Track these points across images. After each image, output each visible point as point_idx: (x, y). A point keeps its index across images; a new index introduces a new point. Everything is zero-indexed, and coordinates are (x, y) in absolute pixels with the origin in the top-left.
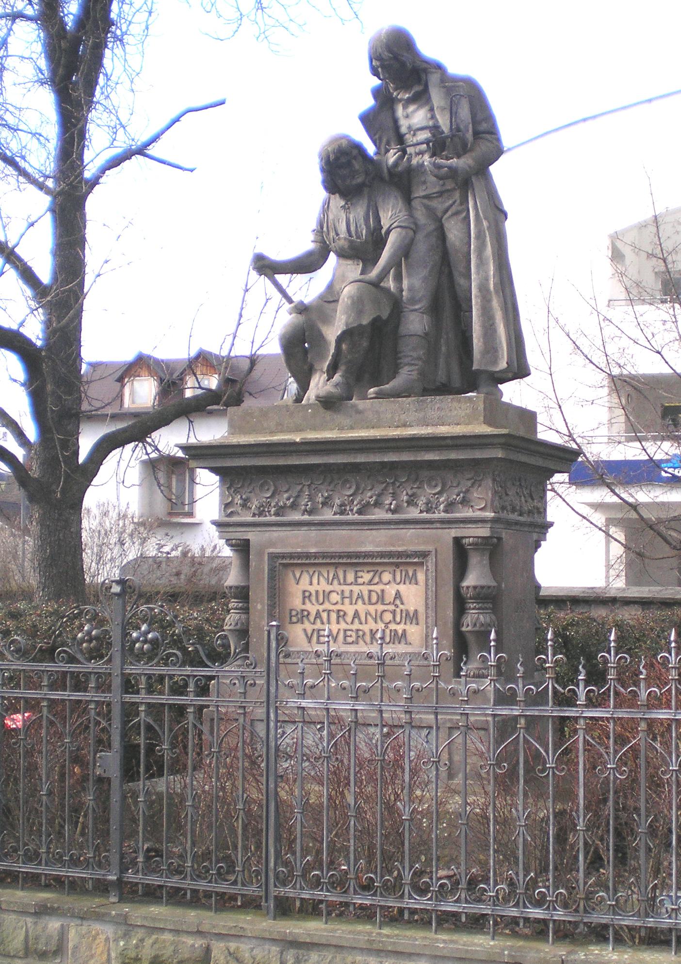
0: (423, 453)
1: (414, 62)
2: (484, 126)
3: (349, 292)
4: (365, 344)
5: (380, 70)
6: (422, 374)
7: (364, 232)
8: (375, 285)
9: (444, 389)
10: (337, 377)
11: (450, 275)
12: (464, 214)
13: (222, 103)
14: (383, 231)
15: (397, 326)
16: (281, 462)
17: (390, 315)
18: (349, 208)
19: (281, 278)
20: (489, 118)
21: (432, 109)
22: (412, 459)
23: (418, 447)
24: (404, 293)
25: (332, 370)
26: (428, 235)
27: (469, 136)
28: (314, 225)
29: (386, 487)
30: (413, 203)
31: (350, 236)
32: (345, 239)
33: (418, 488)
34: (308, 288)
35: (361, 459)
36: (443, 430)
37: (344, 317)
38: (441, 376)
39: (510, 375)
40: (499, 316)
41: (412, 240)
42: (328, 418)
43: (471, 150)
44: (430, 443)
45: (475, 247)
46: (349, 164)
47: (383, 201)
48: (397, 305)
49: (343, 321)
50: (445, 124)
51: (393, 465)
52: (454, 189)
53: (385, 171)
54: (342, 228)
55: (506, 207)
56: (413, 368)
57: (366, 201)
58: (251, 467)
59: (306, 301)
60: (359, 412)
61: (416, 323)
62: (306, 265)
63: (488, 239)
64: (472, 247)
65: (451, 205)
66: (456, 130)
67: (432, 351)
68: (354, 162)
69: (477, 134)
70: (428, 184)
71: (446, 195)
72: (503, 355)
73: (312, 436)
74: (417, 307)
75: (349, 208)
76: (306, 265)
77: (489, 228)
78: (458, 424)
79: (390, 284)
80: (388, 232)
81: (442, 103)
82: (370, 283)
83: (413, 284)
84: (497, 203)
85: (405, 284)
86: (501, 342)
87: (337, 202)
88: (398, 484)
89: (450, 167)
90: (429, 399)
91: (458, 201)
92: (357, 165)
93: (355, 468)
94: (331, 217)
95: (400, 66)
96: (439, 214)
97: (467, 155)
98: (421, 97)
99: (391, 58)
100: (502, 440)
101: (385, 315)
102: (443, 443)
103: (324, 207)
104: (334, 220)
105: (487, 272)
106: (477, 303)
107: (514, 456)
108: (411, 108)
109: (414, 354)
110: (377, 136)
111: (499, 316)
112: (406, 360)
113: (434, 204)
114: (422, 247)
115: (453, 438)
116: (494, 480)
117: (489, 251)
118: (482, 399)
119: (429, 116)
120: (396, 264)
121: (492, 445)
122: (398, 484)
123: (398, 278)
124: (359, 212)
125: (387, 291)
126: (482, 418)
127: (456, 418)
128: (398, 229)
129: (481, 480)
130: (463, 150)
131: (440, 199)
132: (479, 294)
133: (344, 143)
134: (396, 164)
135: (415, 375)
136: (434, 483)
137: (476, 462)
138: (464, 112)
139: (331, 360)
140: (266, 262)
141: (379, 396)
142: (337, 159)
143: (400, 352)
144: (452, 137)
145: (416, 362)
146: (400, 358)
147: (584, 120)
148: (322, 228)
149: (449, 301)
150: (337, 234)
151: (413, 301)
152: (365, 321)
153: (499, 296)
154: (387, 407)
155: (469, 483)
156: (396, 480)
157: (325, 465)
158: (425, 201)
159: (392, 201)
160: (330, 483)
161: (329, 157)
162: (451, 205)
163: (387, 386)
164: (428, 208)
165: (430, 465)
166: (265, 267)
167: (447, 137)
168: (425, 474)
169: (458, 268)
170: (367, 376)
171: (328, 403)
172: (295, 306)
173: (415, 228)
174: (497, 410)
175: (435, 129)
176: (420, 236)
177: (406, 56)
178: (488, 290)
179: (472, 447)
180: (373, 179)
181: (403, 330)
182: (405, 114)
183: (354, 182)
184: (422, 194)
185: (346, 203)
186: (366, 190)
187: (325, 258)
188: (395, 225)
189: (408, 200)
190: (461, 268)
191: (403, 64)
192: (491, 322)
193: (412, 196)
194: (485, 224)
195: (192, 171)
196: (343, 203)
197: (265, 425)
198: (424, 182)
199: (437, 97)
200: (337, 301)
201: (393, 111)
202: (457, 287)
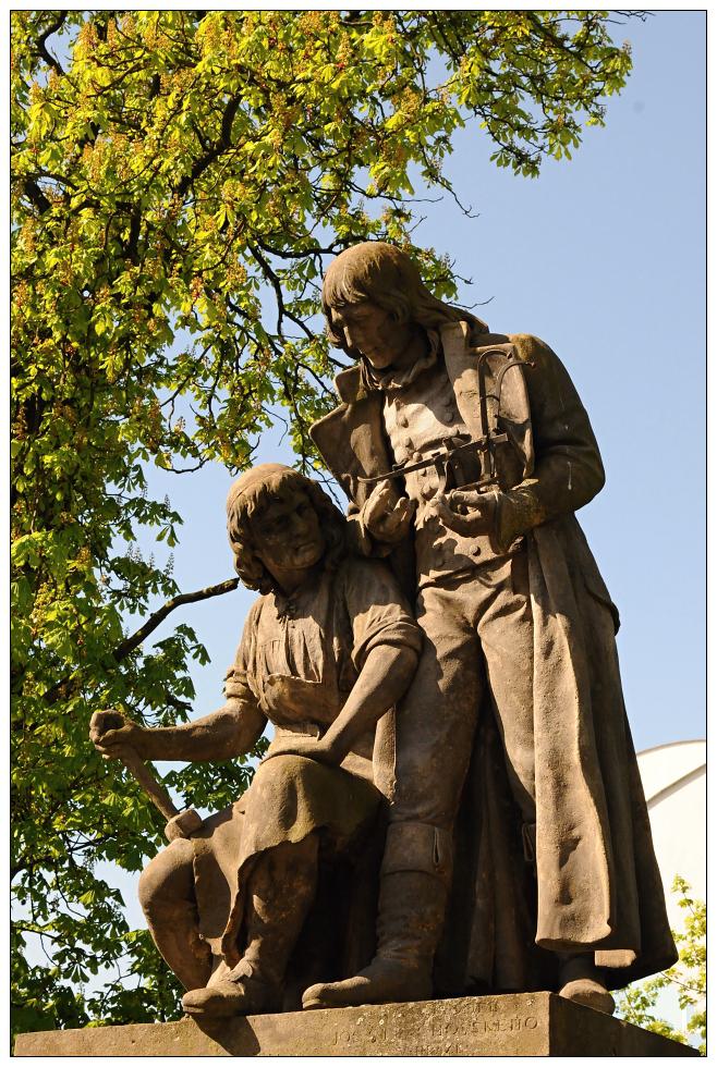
4: (303, 889)
12: (521, 612)
14: (354, 654)
48: (375, 811)
57: (325, 600)
61: (416, 844)
64: (535, 673)
68: (296, 518)
84: (594, 589)
98: (430, 384)
124: (308, 629)
132: (549, 772)
141: (329, 1000)
142: (258, 512)
161: (244, 510)
164: (447, 602)
181: (391, 861)
182: (401, 420)
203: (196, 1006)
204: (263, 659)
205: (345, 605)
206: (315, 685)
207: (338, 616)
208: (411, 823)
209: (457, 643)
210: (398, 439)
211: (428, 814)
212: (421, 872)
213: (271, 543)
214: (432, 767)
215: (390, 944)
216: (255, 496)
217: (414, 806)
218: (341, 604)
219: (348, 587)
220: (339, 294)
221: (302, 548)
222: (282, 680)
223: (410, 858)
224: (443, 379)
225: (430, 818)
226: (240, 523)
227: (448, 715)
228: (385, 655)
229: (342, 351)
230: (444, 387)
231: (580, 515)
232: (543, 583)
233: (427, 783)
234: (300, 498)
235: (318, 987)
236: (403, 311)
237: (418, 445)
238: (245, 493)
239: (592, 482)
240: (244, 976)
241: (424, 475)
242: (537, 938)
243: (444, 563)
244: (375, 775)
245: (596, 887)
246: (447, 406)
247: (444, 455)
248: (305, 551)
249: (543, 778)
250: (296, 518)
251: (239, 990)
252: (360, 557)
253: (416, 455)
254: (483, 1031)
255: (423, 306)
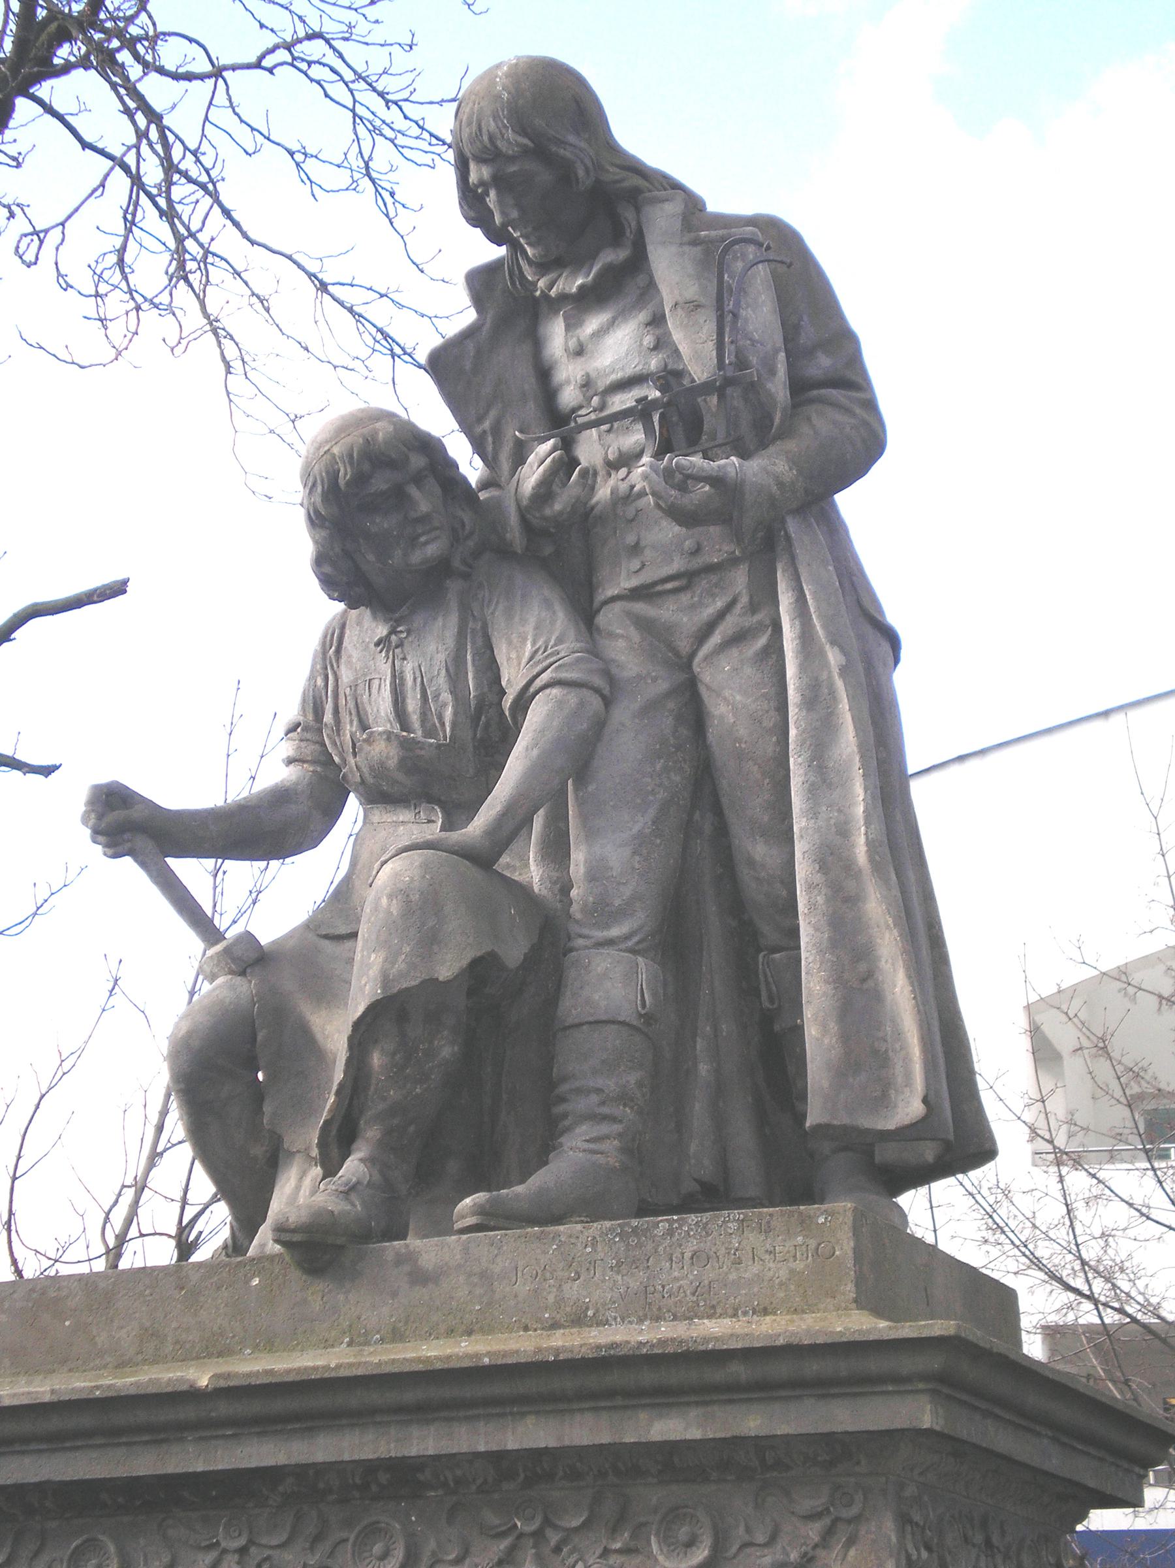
0: (643, 1415)
1: (598, 167)
2: (823, 364)
3: (396, 875)
5: (492, 199)
6: (633, 1150)
7: (448, 713)
8: (483, 858)
9: (712, 1195)
10: (353, 1167)
11: (722, 831)
12: (762, 641)
13: (117, 589)
15: (552, 1001)
16: (145, 1463)
17: (531, 961)
18: (400, 645)
19: (192, 871)
20: (843, 341)
21: (657, 320)
22: (605, 1439)
23: (627, 1393)
24: (574, 893)
25: (338, 1140)
26: (650, 708)
27: (778, 387)
28: (291, 709)
29: (512, 1549)
30: (601, 619)
31: (405, 725)
32: (389, 736)
33: (627, 1551)
34: (277, 899)
35: (424, 1442)
36: (714, 1329)
37: (376, 960)
38: (699, 1158)
39: (929, 1153)
40: (888, 948)
41: (599, 726)
42: (316, 1305)
43: (785, 433)
44: (673, 1377)
45: (801, 733)
46: (398, 496)
47: (509, 615)
48: (551, 936)
49: (374, 972)
50: (697, 356)
51: (539, 1466)
52: (733, 561)
53: (513, 519)
54: (381, 705)
55: (893, 616)
56: (604, 1128)
57: (453, 619)
58: (41, 1487)
59: (266, 936)
60: (420, 1278)
61: (611, 981)
62: (261, 831)
63: (844, 705)
64: (793, 732)
65: (721, 615)
66: (735, 377)
67: (667, 1080)
68: (413, 491)
69: (800, 387)
70: (648, 554)
71: (703, 583)
72: (908, 1075)
73: (252, 1365)
74: (615, 932)
75: (400, 645)
76: (261, 831)
77: (844, 671)
78: (765, 1312)
79: (534, 873)
80: (523, 702)
81: (691, 291)
82: (467, 853)
83: (604, 861)
84: (866, 603)
85: (578, 858)
86: (899, 1034)
87: (368, 628)
88: (554, 1538)
89: (717, 481)
90: (662, 1223)
91: (744, 600)
92: (423, 502)
93: (401, 1480)
94: (346, 676)
95: (553, 180)
96: (684, 646)
97: (772, 449)
99: (525, 151)
100: (933, 1363)
101: (514, 952)
102: (717, 1375)
103: (324, 652)
104: (354, 686)
105: (843, 811)
106: (812, 906)
107: (975, 1429)
108: (593, 324)
109: (610, 1084)
110: (487, 425)
111: (888, 948)
112: (581, 1104)
113: (667, 612)
114: (629, 745)
115: (749, 1354)
116: (904, 1520)
117: (848, 741)
118: (849, 1219)
119: (649, 340)
120: (550, 795)
121: (897, 1379)
122: (554, 1538)
123: (557, 849)
124: (432, 651)
125: (522, 891)
126: (849, 1289)
127: (755, 1283)
128: (555, 691)
129: (857, 1519)
130: (759, 433)
131: (685, 598)
132: (818, 878)
133: (383, 430)
134: (545, 491)
135: (611, 1153)
136: (683, 1532)
137: (836, 1450)
138: (761, 316)
139: (337, 1104)
140: (136, 813)
141: (492, 1220)
142: (360, 479)
143: (564, 1079)
144: (719, 387)
145: (618, 1110)
146: (562, 1099)
147: (961, 758)
148: (318, 713)
149: (720, 917)
150: (364, 727)
151: (602, 912)
152: (447, 967)
153: (887, 882)
154: (515, 1256)
155: (813, 1531)
156: (547, 1522)
157: (301, 1472)
158: (640, 607)
159: (534, 614)
160: (317, 1539)
161: (333, 476)
162: (721, 615)
163: (519, 1189)
164: (645, 625)
165: (670, 1460)
166: (128, 824)
167: (707, 388)
168: (653, 1496)
169: (747, 806)
170: (453, 1167)
171: (319, 1250)
172: (227, 951)
173: (609, 691)
174: (901, 1268)
175: (670, 377)
176: (623, 713)
177: (574, 145)
178: (849, 867)
179: (822, 1388)
180: (477, 554)
181: (570, 1008)
182: (572, 343)
183: (416, 557)
184: (627, 583)
185: (393, 631)
186: (454, 587)
187: (332, 813)
188: (545, 677)
189: (585, 612)
190: (757, 805)
191: (565, 173)
192: (863, 967)
193: (600, 597)
194: (834, 657)
195: (47, 771)
196: (382, 631)
197: (102, 1339)
198: (636, 549)
199: (671, 271)
200: (354, 935)
201: (537, 344)
202: (745, 873)
203: (294, 1231)
204: (351, 705)
205: (485, 627)
206: (439, 746)
207: (473, 643)
208: (604, 951)
209: (663, 686)
210: (569, 376)
211: (627, 937)
212: (623, 1023)
213: (374, 529)
214: (633, 868)
215: (577, 1131)
216: (351, 456)
217: (607, 926)
218: (479, 625)
219: (490, 601)
220: (485, 138)
221: (423, 539)
222: (388, 739)
223: (603, 1003)
224: (641, 280)
225: (630, 944)
226: (325, 496)
227: (653, 792)
228: (560, 703)
229: (478, 232)
230: (642, 295)
231: (846, 501)
232: (801, 599)
233: (627, 892)
234: (418, 461)
235: (480, 1197)
236: (587, 170)
237: (601, 385)
238: (336, 450)
239: (863, 447)
240: (358, 1183)
241: (609, 431)
242: (808, 1124)
243: (643, 566)
244: (536, 880)
245: (897, 1046)
246: (647, 325)
247: (655, 401)
248: (426, 543)
249: (810, 887)
250: (413, 491)
251: (353, 1205)
252: (504, 552)
253: (596, 400)
254: (750, 1263)
255: (612, 164)
